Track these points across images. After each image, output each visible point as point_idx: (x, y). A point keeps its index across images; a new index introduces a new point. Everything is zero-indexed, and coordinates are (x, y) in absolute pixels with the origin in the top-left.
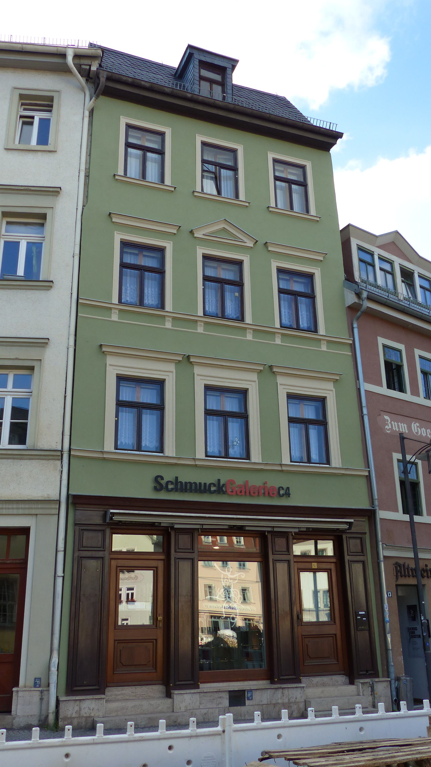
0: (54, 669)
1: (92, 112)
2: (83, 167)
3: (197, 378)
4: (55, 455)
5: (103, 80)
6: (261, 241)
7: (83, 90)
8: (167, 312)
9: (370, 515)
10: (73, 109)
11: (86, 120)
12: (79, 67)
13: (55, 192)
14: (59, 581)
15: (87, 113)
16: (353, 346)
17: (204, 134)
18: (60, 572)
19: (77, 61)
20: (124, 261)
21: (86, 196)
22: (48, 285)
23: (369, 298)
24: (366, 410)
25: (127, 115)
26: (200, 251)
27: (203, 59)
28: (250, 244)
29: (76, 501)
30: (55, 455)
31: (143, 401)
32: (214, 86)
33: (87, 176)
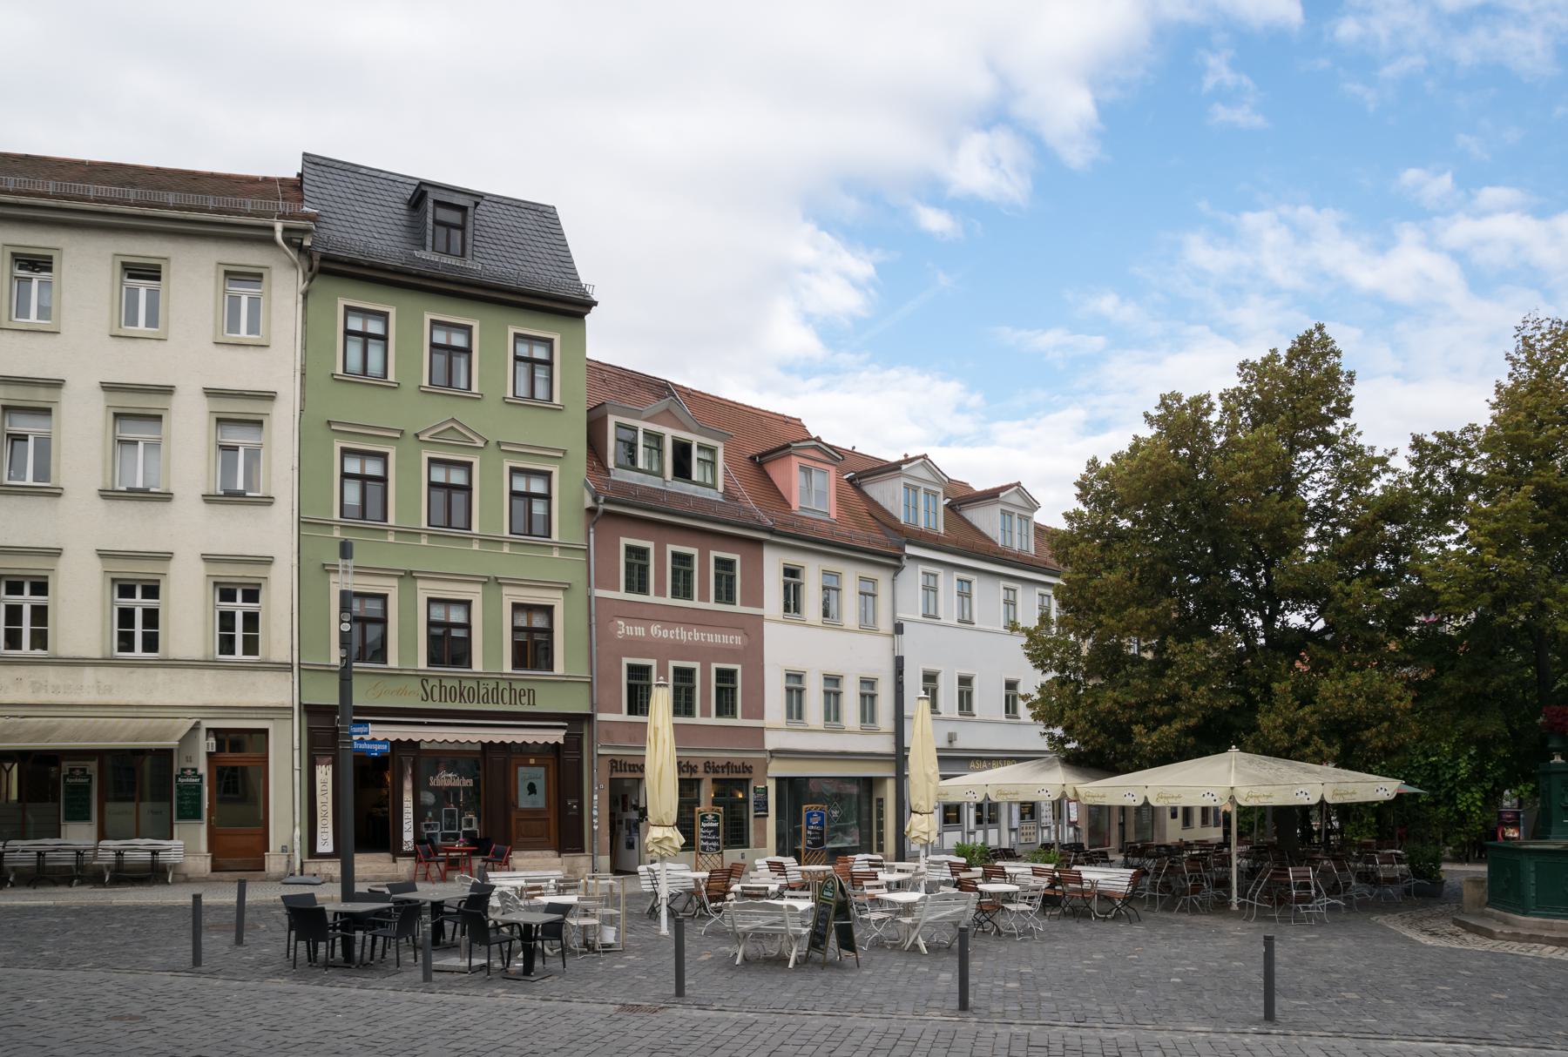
0: (297, 840)
1: (305, 296)
2: (298, 367)
3: (420, 592)
4: (286, 667)
5: (317, 257)
6: (492, 442)
7: (295, 266)
8: (695, 483)
9: (589, 718)
10: (285, 288)
11: (300, 306)
12: (287, 241)
13: (270, 397)
14: (297, 774)
15: (300, 297)
16: (587, 551)
17: (431, 312)
18: (297, 766)
19: (287, 235)
20: (432, 618)
21: (303, 399)
22: (268, 501)
23: (607, 501)
24: (598, 616)
25: (344, 297)
26: (426, 455)
27: (439, 198)
28: (481, 444)
29: (310, 711)
30: (286, 667)
31: (366, 638)
32: (453, 231)
33: (303, 375)
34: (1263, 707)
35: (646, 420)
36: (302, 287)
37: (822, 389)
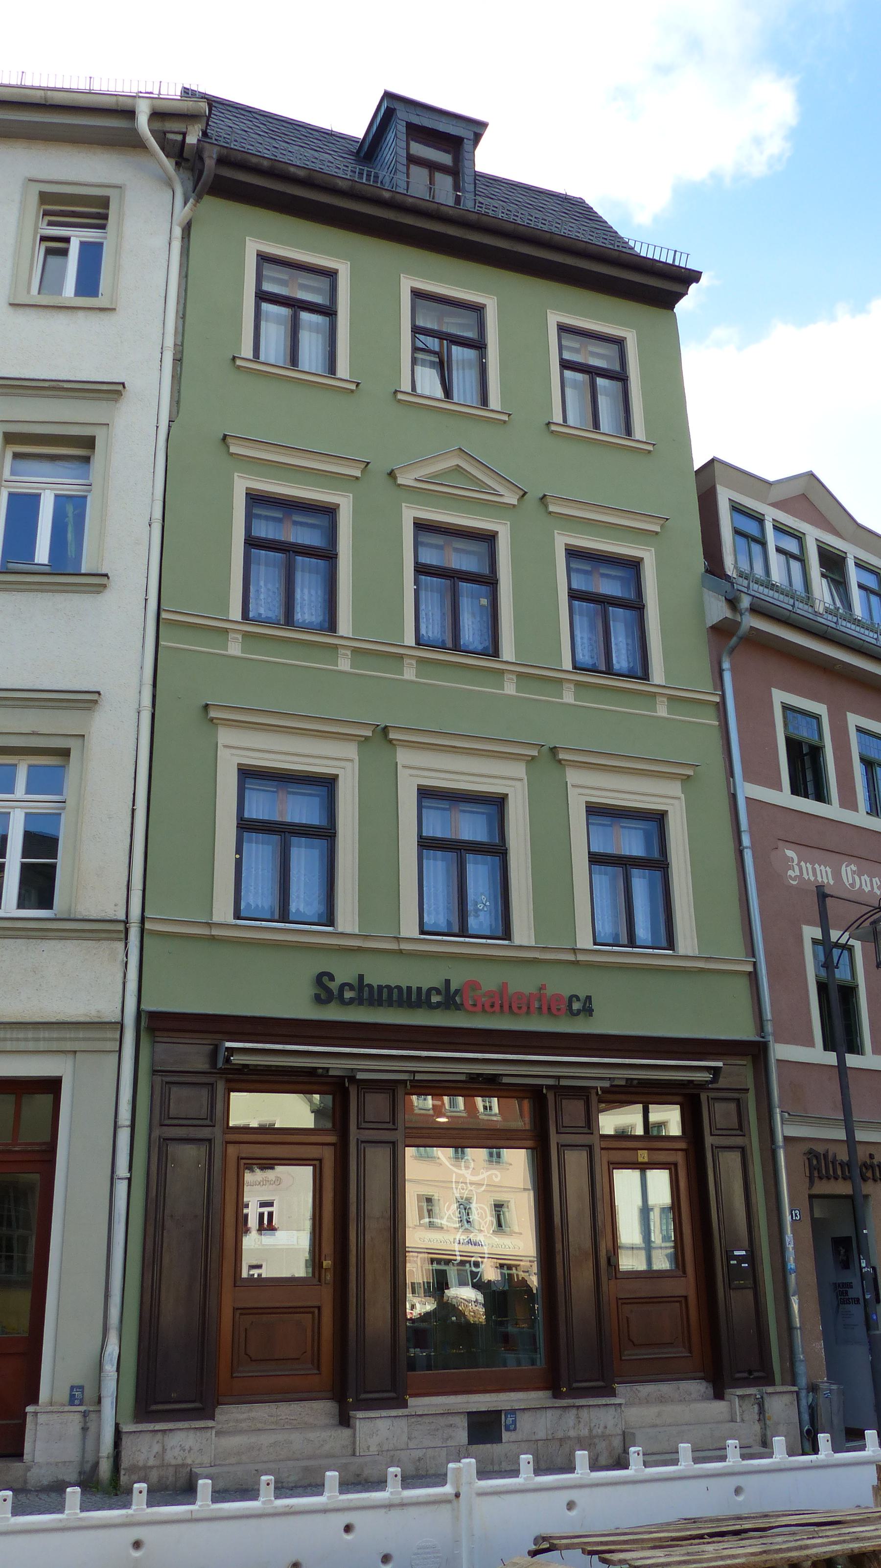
1: (187, 229)
2: (170, 342)
3: (402, 773)
4: (113, 930)
5: (210, 163)
6: (535, 493)
7: (169, 184)
9: (756, 1052)
10: (149, 222)
11: (177, 245)
12: (161, 138)
13: (113, 392)
14: (121, 1188)
15: (178, 232)
16: (721, 708)
17: (416, 274)
18: (122, 1170)
19: (158, 125)
21: (176, 401)
22: (98, 582)
23: (755, 610)
24: (749, 837)
25: (260, 236)
26: (409, 514)
27: (415, 120)
28: (511, 498)
29: (156, 1025)
30: (113, 930)
32: (438, 176)
33: (178, 360)
34: (514, 1271)
35: (775, 505)
36: (182, 212)
37: (491, 925)
